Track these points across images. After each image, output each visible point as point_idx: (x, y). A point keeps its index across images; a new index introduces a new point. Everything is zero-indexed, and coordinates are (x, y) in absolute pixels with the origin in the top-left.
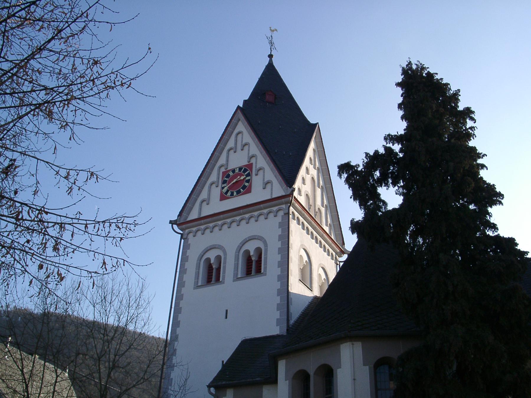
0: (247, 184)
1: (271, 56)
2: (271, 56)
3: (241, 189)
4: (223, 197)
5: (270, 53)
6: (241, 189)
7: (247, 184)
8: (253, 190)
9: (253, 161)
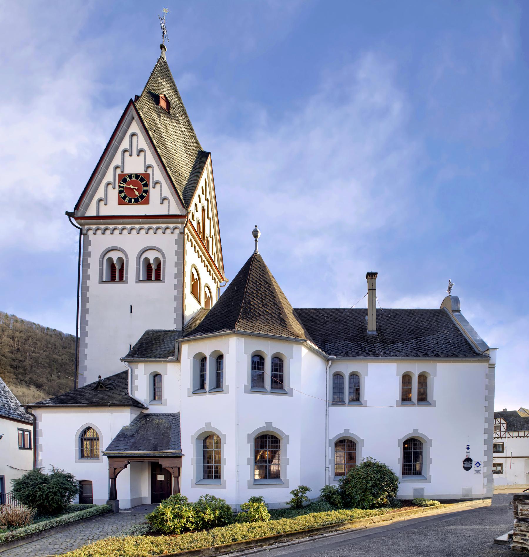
0: (144, 195)
3: (139, 199)
4: (121, 202)
6: (139, 199)
8: (151, 202)
9: (150, 171)
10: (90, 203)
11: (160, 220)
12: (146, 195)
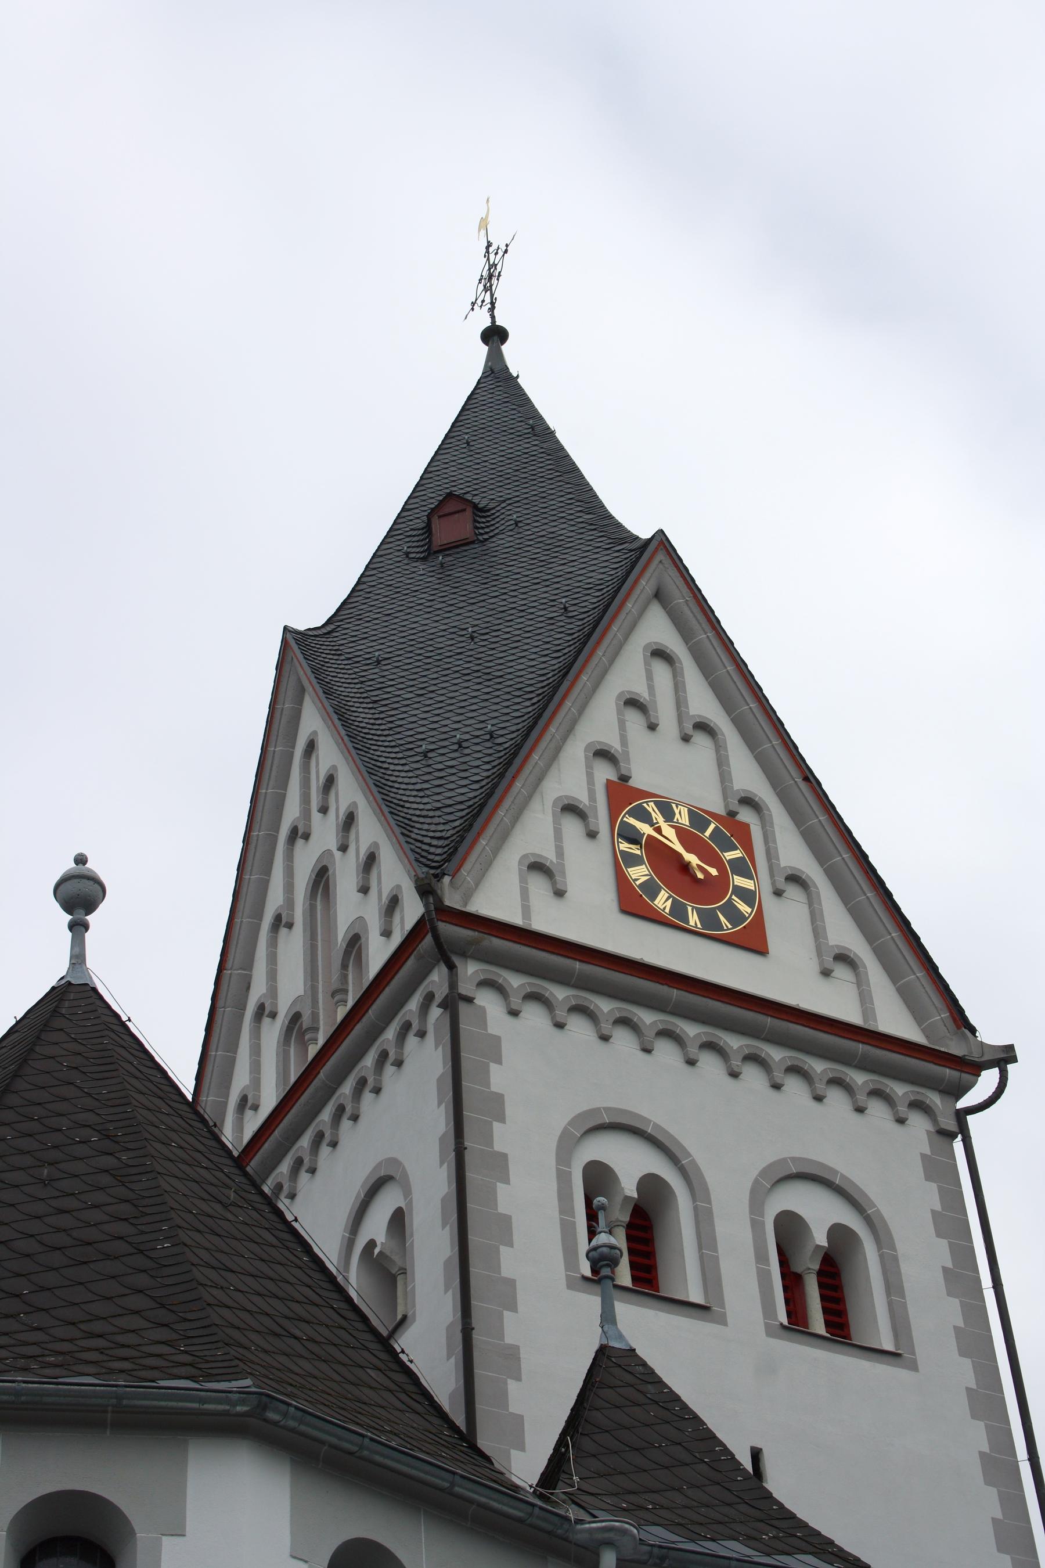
1: (494, 336)
2: (494, 336)
5: (488, 323)
7: (744, 908)
10: (495, 857)
11: (578, 965)
12: (749, 910)
